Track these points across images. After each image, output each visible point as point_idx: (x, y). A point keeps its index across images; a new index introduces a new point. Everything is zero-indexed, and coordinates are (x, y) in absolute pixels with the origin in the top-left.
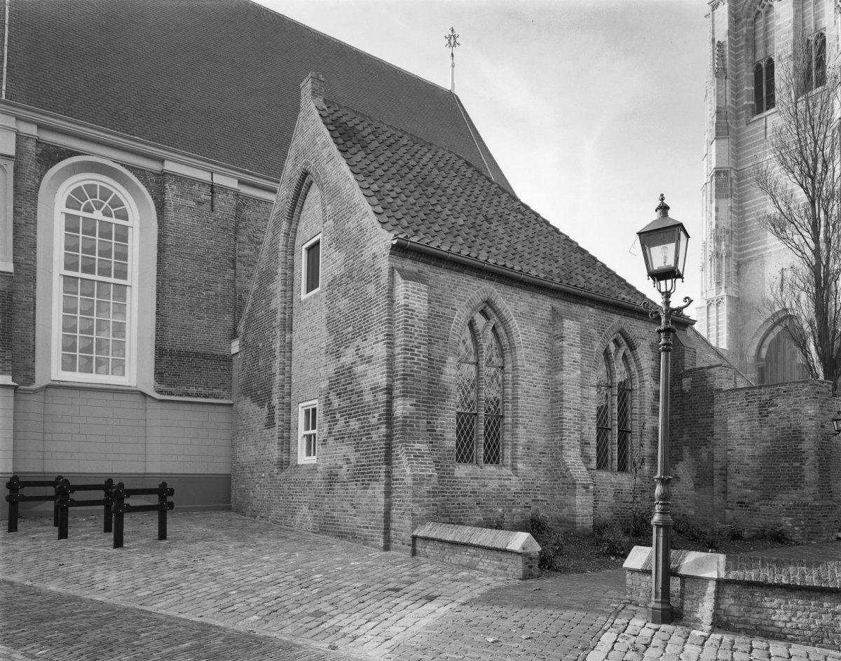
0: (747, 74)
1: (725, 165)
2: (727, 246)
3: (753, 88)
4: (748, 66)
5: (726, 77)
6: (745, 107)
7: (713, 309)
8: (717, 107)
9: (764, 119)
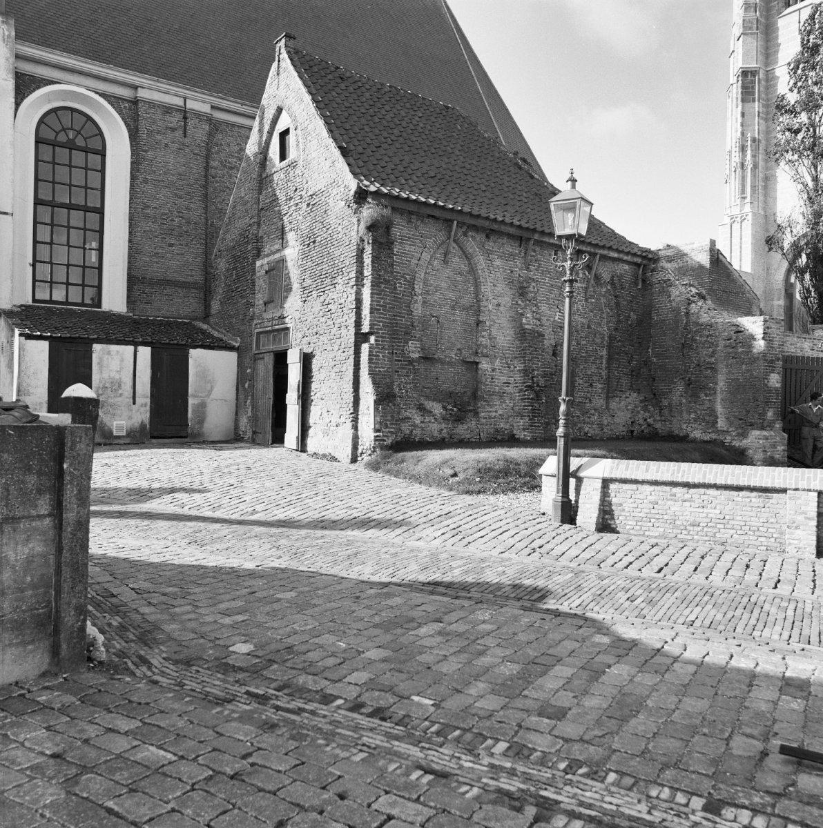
7: (736, 226)
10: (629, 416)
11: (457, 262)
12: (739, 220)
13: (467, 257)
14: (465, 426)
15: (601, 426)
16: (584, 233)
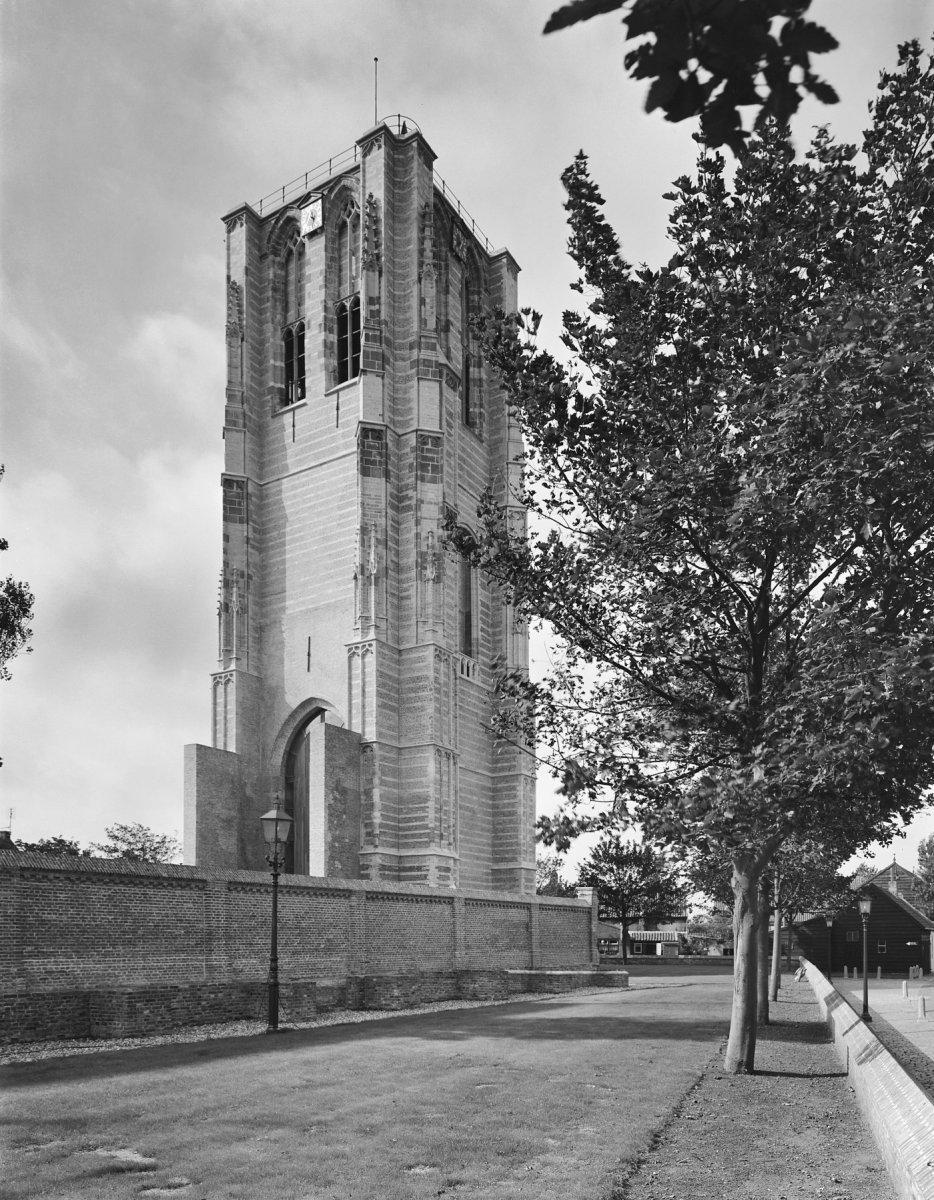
0: (275, 342)
1: (376, 420)
2: (240, 596)
3: (283, 365)
4: (275, 330)
5: (242, 340)
7: (357, 661)
8: (515, 279)
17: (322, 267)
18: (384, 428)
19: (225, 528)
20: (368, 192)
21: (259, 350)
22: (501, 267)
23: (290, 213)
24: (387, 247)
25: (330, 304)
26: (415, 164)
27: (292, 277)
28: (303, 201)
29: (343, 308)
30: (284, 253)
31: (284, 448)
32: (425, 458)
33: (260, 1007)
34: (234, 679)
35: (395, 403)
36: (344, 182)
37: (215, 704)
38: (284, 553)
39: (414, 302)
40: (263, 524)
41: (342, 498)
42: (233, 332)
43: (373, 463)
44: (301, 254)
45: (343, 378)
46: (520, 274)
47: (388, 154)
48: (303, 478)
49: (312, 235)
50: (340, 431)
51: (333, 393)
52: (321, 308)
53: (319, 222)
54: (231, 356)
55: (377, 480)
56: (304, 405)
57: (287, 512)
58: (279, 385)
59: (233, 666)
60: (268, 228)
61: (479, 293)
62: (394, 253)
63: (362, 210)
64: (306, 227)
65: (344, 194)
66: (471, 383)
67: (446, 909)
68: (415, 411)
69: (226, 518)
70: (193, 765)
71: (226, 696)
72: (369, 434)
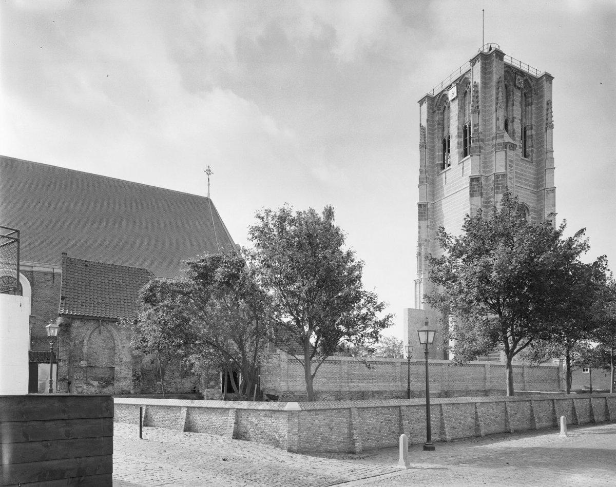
1: (477, 174)
4: (439, 140)
6: (437, 165)
7: (418, 285)
8: (551, 83)
9: (462, 164)
10: (192, 385)
11: (105, 333)
12: (418, 282)
13: (109, 331)
14: (107, 389)
15: (177, 389)
16: (56, 335)
17: (457, 112)
18: (480, 176)
19: (419, 223)
20: (474, 81)
21: (432, 151)
22: (543, 82)
23: (444, 93)
24: (482, 102)
25: (460, 126)
26: (494, 63)
27: (446, 117)
28: (450, 87)
29: (466, 127)
30: (442, 108)
31: (443, 187)
32: (498, 184)
33: (424, 395)
34: (422, 281)
35: (486, 164)
36: (466, 76)
37: (416, 291)
38: (443, 222)
39: (494, 120)
40: (434, 218)
41: (464, 205)
42: (423, 146)
43: (475, 191)
44: (449, 107)
45: (466, 155)
46: (554, 81)
47: (482, 63)
48: (449, 199)
49: (453, 100)
50: (464, 177)
51: (461, 163)
52: (456, 129)
53: (455, 95)
54: (421, 156)
55: (477, 198)
56: (450, 169)
57: (444, 213)
58: (440, 162)
59: (422, 277)
60: (436, 100)
61: (531, 97)
62: (485, 107)
63: (472, 89)
64: (450, 98)
65: (466, 80)
66: (527, 138)
67: (482, 369)
68: (494, 163)
69: (419, 220)
70: (407, 316)
71: (420, 288)
72: (474, 181)
